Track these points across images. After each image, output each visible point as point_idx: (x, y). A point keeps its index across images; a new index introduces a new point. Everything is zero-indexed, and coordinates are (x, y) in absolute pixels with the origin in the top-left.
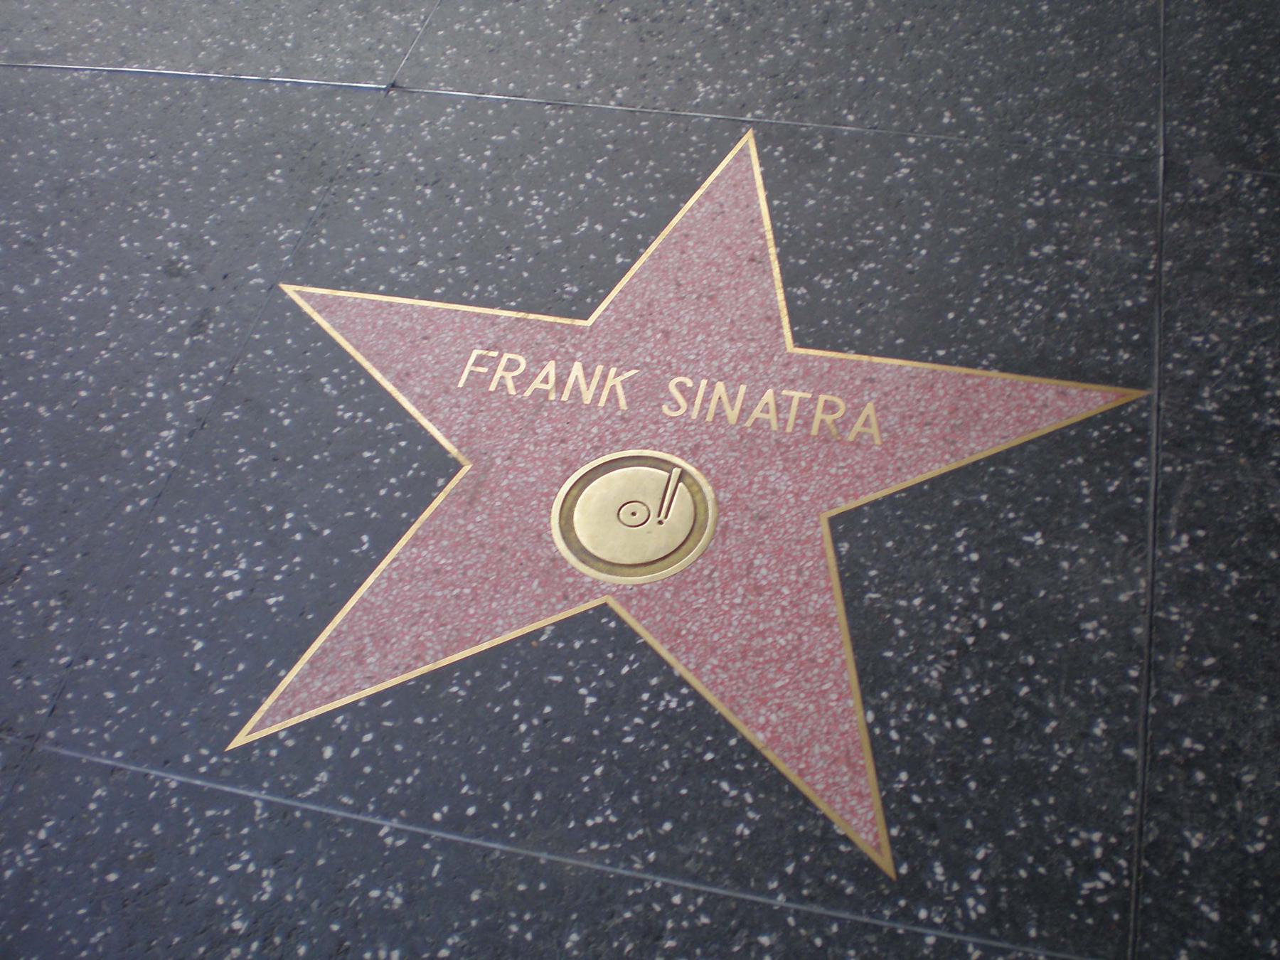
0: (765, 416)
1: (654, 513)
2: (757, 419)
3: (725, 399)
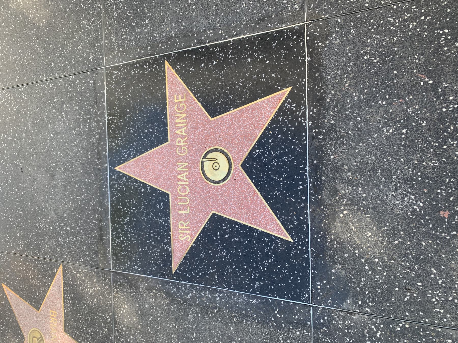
0: (183, 131)
2: (186, 178)
3: (180, 118)
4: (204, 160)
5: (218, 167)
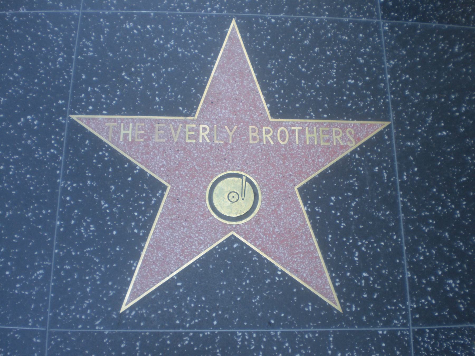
1: (240, 196)
4: (244, 178)
5: (230, 199)
